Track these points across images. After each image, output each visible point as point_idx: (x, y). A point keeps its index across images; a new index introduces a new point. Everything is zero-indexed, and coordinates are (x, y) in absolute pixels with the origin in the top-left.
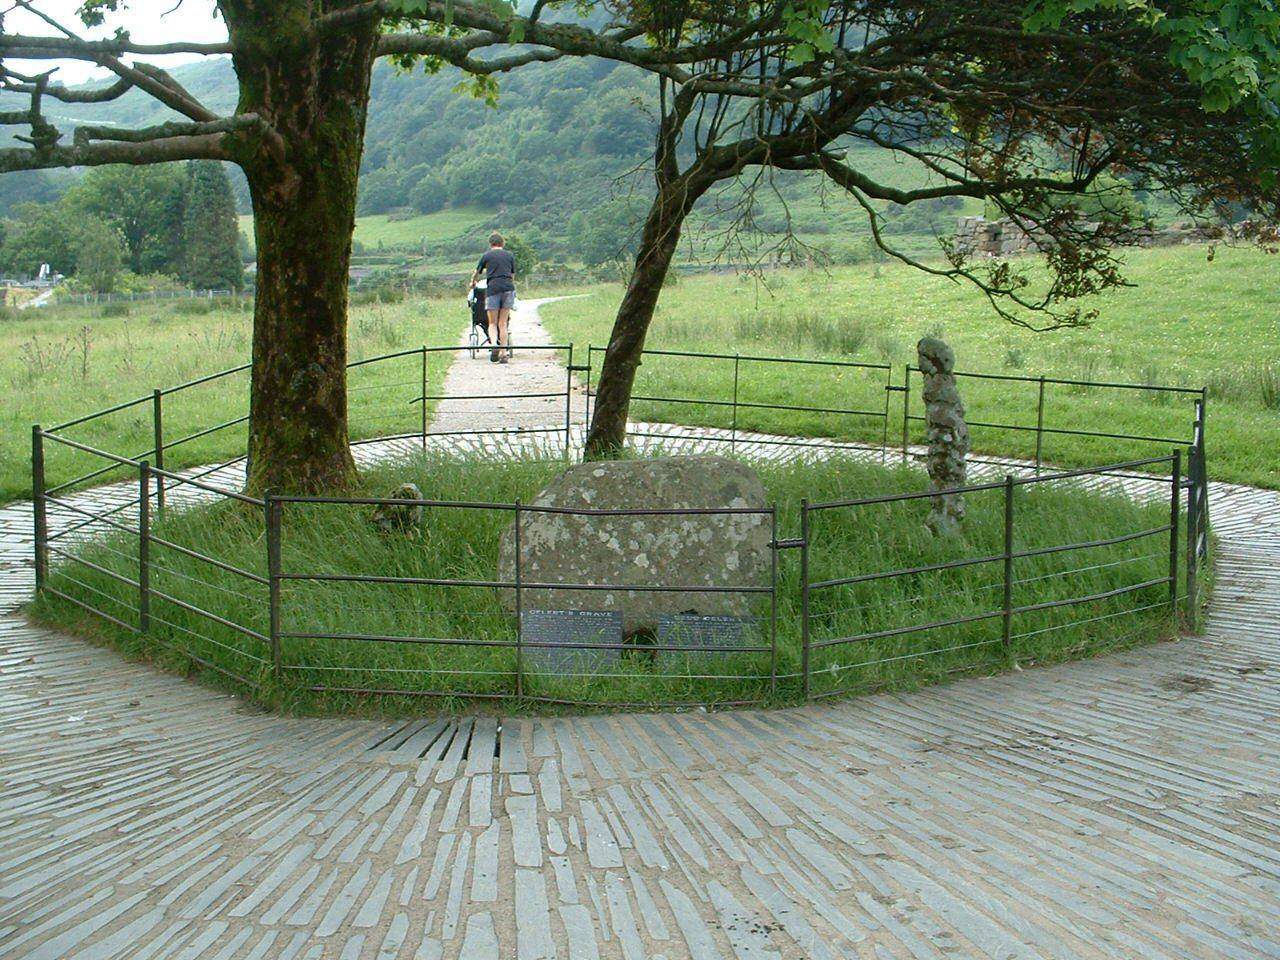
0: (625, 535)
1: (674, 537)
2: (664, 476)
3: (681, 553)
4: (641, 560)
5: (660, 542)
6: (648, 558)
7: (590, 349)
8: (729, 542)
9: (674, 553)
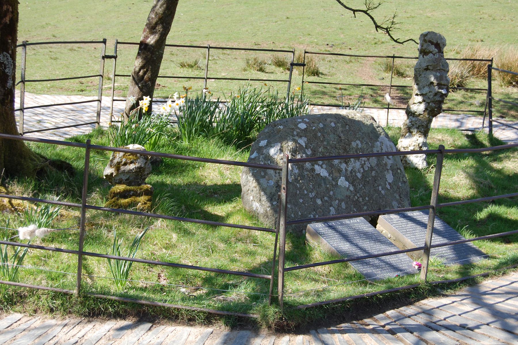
3: (363, 175)
4: (342, 182)
5: (350, 169)
6: (347, 180)
9: (359, 175)
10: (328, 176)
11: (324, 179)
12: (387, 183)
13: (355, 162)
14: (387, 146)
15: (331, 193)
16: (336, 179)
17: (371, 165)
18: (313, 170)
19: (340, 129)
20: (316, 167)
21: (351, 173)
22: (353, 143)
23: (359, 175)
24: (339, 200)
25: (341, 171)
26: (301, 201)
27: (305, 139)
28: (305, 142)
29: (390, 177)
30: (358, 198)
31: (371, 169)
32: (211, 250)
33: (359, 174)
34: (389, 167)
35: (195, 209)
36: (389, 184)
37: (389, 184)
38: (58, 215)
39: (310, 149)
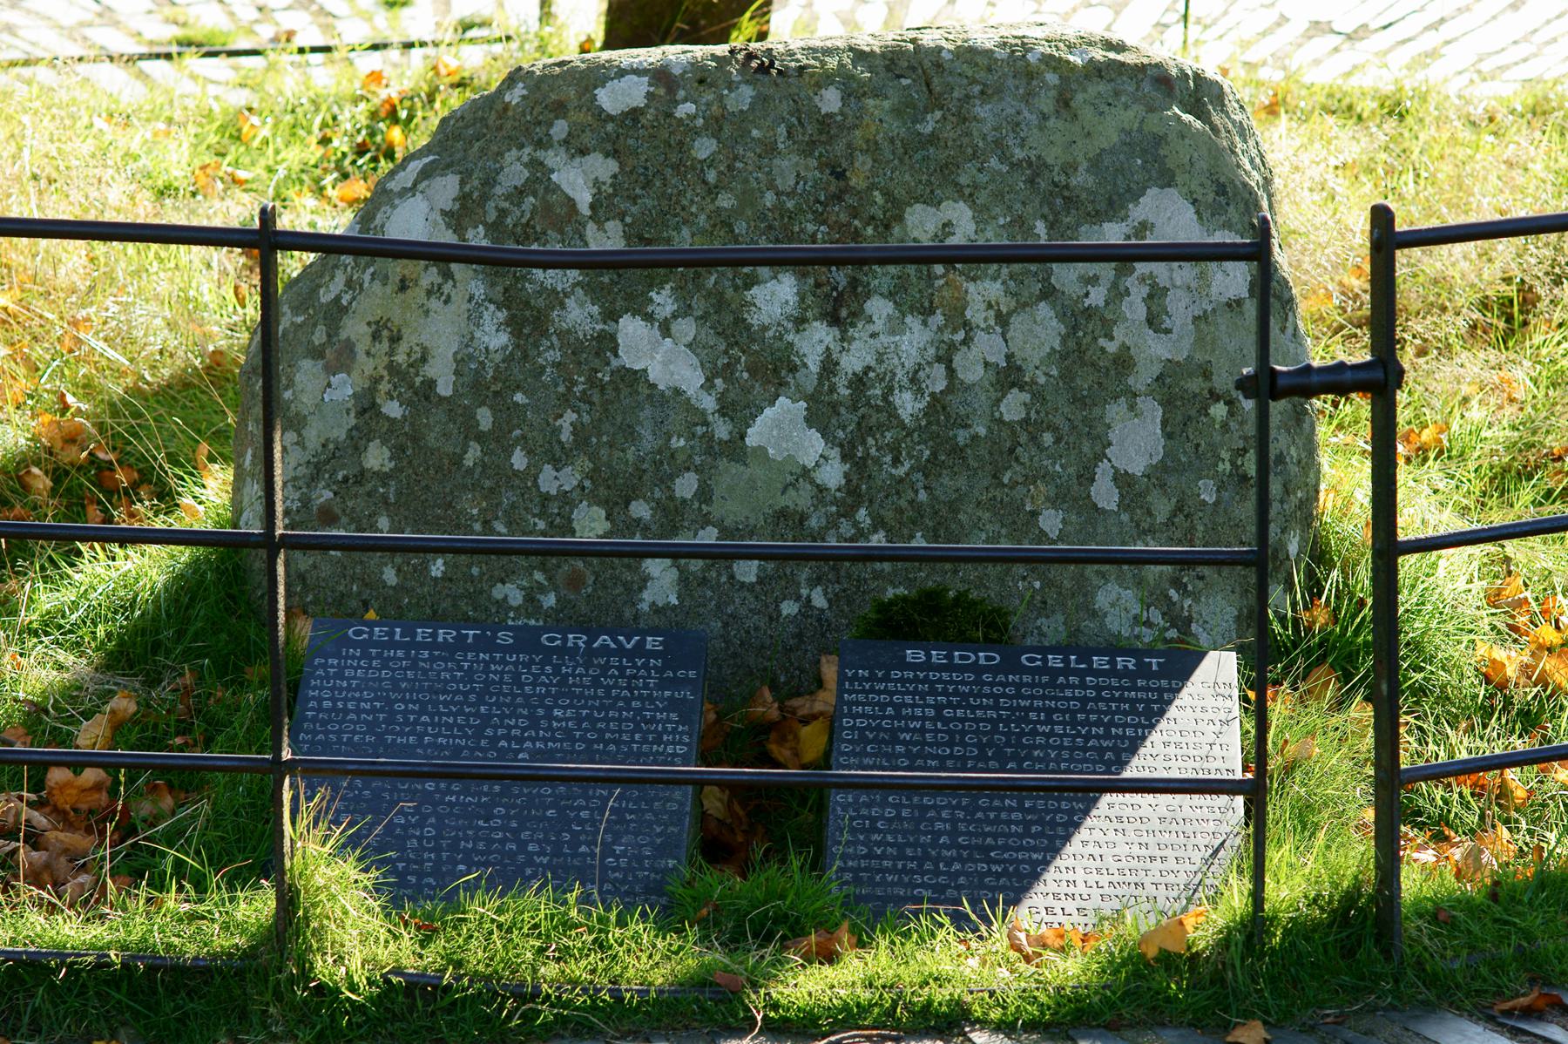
3: (937, 405)
5: (853, 361)
8: (1124, 361)
9: (908, 405)
13: (896, 327)
18: (607, 343)
20: (631, 329)
21: (859, 382)
23: (908, 405)
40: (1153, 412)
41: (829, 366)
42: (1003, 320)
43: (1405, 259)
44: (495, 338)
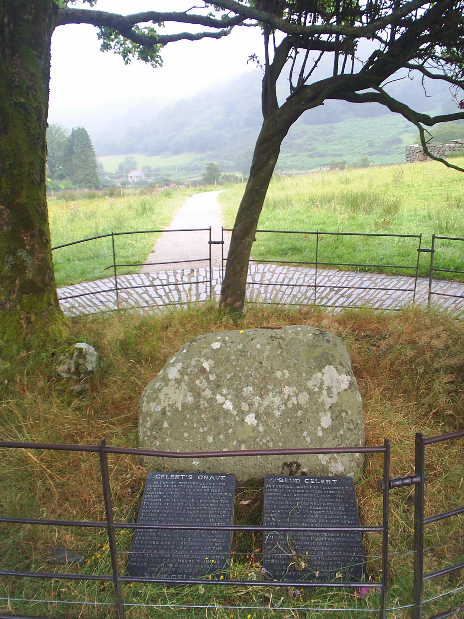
0: (238, 398)
1: (277, 400)
2: (268, 347)
3: (283, 414)
4: (250, 419)
5: (265, 404)
7: (223, 230)
8: (323, 404)
9: (277, 414)
10: (231, 409)
11: (227, 413)
12: (319, 428)
13: (274, 396)
14: (322, 383)
15: (231, 431)
16: (243, 414)
17: (298, 402)
19: (266, 354)
22: (245, 389)
23: (277, 414)
24: (238, 441)
25: (252, 405)
26: (186, 435)
27: (211, 362)
28: (210, 366)
29: (326, 421)
30: (268, 441)
31: (298, 407)
32: (91, 216)
33: (277, 411)
34: (327, 407)
35: (59, 313)
36: (323, 429)
37: (323, 429)
38: (293, 610)
39: (214, 375)
40: (329, 414)
41: (260, 405)
42: (297, 395)
43: (208, 258)
44: (190, 399)
